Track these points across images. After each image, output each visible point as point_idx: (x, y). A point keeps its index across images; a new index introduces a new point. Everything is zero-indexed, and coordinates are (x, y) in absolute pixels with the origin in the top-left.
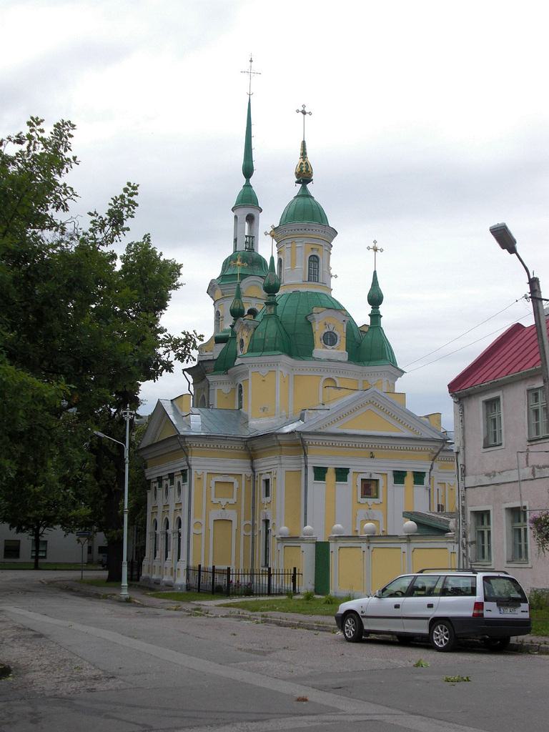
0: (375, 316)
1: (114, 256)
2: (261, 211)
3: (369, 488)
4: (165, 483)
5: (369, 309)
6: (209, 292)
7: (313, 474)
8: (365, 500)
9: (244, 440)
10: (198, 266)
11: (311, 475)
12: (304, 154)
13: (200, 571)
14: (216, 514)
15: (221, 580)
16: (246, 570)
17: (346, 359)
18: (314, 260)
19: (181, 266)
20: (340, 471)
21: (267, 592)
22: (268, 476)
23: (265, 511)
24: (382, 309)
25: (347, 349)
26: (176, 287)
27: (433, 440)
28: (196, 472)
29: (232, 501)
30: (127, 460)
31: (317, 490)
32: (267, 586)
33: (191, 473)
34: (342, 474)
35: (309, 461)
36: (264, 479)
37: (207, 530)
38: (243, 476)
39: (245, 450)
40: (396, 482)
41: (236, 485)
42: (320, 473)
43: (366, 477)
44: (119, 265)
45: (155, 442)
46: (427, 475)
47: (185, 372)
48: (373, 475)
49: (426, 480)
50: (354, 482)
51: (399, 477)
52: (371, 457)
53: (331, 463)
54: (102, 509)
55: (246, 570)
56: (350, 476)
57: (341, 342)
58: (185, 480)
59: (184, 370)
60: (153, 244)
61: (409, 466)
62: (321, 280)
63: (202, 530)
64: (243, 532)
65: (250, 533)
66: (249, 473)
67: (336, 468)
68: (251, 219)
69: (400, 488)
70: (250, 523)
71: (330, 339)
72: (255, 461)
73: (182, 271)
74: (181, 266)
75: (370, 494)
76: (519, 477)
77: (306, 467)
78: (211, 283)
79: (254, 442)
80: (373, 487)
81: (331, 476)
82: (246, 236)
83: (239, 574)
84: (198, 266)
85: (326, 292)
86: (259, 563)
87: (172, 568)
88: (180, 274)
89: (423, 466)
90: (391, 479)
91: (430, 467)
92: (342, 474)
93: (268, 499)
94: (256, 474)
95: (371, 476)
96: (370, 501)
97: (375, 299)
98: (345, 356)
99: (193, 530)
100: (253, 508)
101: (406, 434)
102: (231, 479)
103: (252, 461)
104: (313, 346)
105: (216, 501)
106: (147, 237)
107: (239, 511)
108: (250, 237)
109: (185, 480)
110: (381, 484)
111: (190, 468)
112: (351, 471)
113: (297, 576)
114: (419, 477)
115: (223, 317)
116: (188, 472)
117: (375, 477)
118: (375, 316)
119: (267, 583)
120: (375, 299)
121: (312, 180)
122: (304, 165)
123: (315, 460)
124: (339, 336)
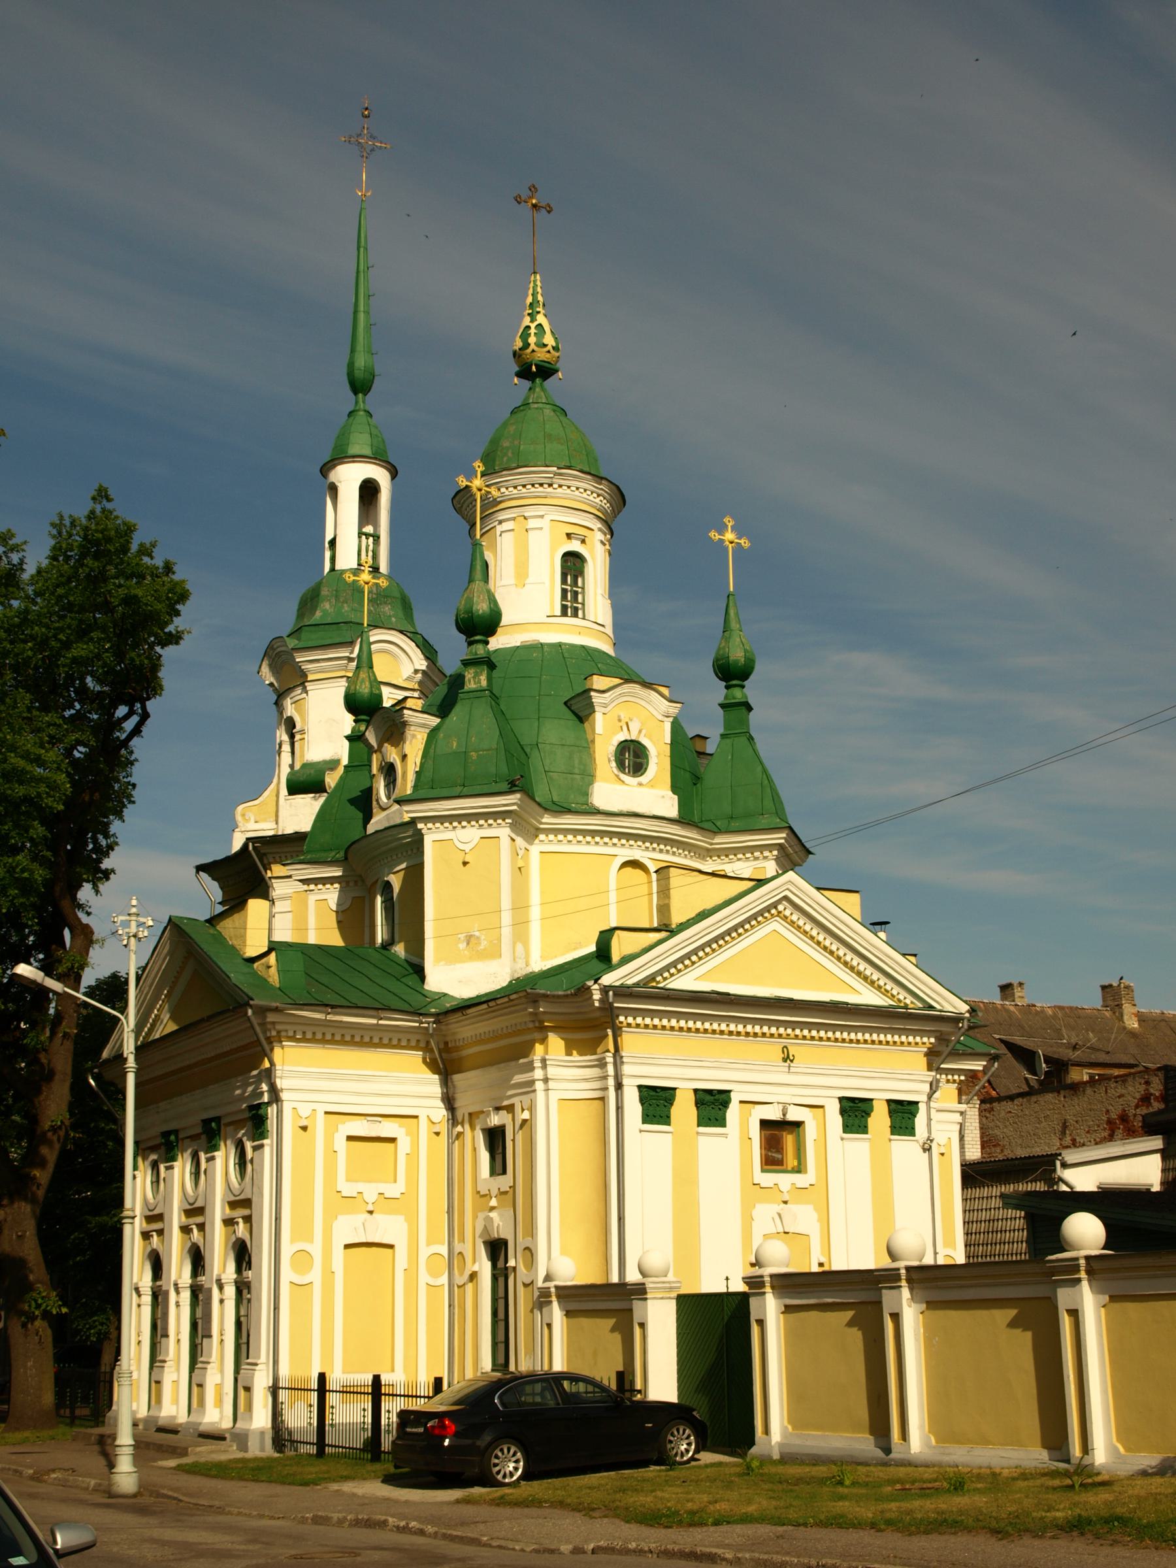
1: (721, 532)
3: (779, 1139)
7: (639, 1108)
8: (768, 1179)
14: (350, 1228)
17: (673, 813)
20: (708, 1098)
25: (675, 789)
29: (393, 1190)
30: (131, 1062)
31: (648, 1150)
35: (626, 1069)
37: (329, 1274)
38: (423, 1120)
40: (847, 1128)
41: (404, 1144)
42: (657, 1103)
43: (774, 1114)
44: (745, 543)
46: (922, 1107)
48: (791, 1109)
49: (920, 1121)
50: (742, 1127)
51: (855, 1113)
52: (785, 1060)
56: (733, 1113)
59: (200, 868)
63: (315, 1276)
65: (444, 1280)
67: (696, 1091)
69: (858, 1145)
70: (444, 1250)
75: (780, 1162)
76: (329, 1446)
77: (619, 1086)
80: (789, 1140)
81: (684, 1109)
92: (713, 1106)
96: (785, 1181)
99: (287, 1275)
100: (450, 1211)
101: (869, 997)
102: (386, 1129)
105: (348, 1189)
110: (811, 1132)
112: (735, 1098)
114: (903, 1115)
115: (302, 732)
117: (793, 1115)
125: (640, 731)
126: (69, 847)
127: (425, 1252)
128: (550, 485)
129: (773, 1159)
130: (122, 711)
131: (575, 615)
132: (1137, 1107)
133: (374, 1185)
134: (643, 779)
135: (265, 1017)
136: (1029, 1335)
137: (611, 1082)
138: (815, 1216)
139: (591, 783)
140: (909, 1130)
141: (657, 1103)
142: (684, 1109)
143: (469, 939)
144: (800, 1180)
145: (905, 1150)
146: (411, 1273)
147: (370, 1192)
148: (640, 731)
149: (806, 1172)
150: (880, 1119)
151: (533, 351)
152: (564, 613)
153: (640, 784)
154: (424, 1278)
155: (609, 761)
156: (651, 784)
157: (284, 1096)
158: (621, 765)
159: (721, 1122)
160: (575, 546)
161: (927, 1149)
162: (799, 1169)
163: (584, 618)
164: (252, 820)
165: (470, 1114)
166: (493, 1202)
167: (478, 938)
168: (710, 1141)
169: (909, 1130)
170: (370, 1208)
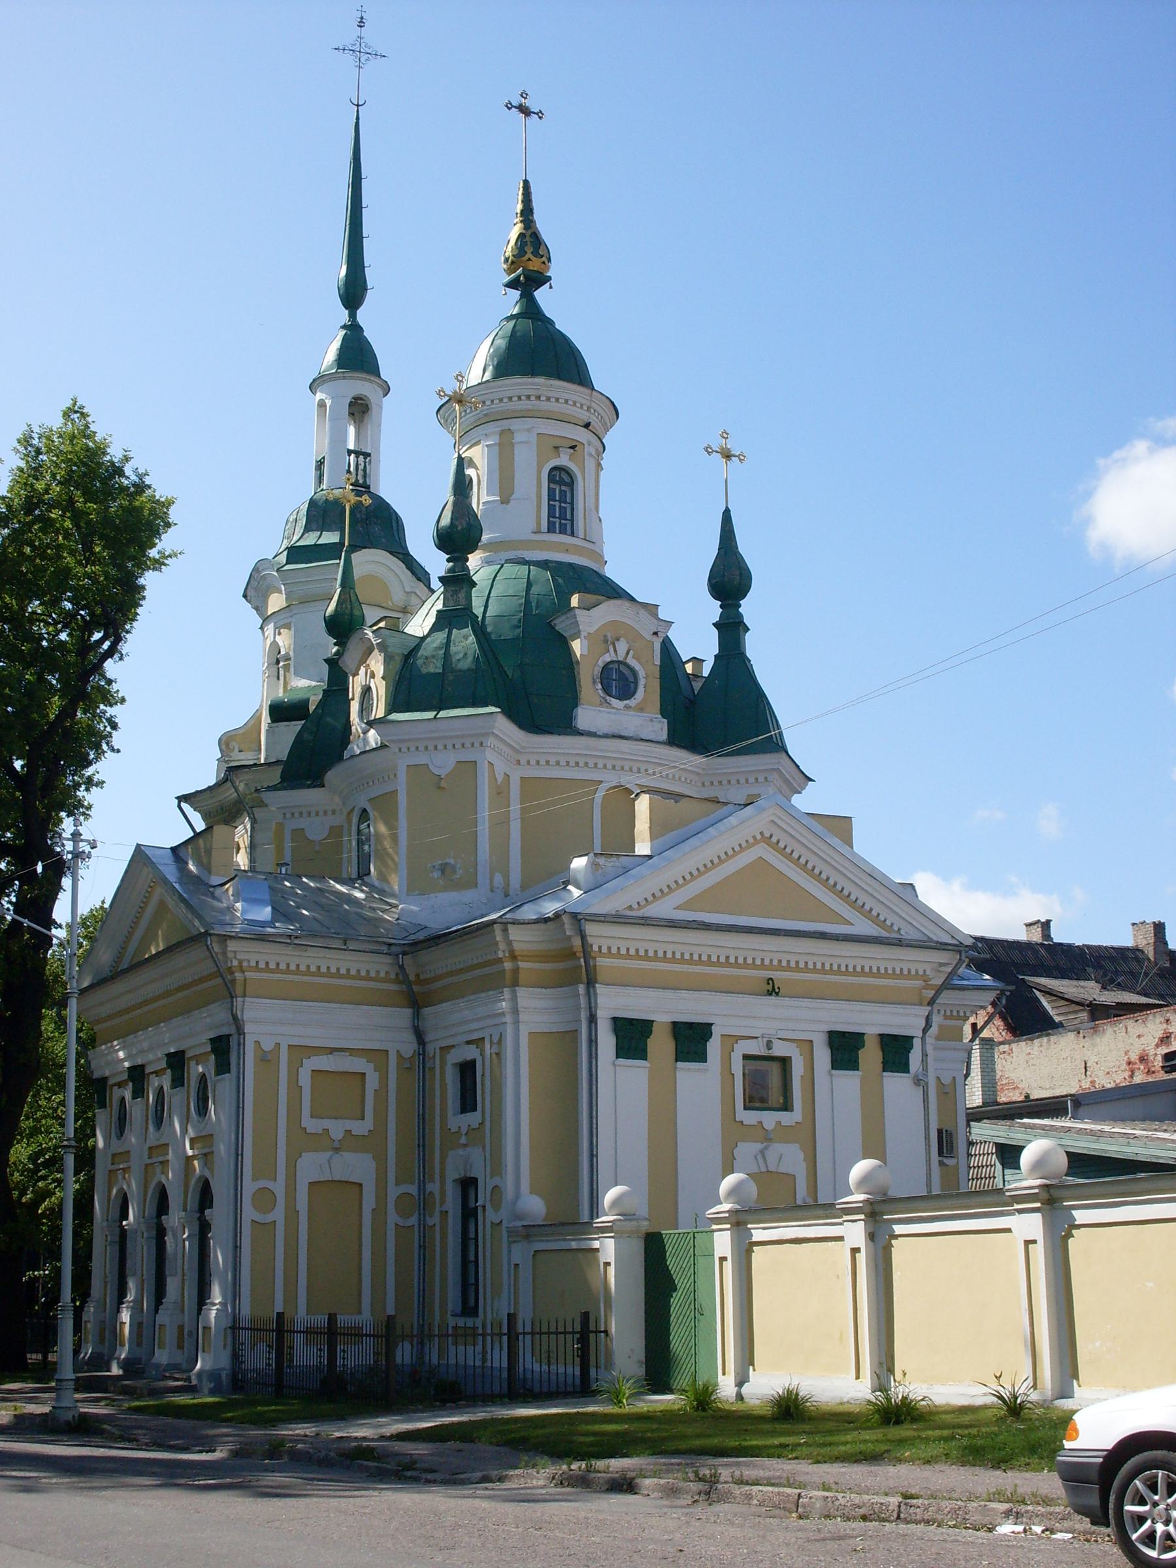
0: (731, 629)
2: (387, 390)
3: (768, 1082)
4: (154, 1082)
5: (714, 609)
6: (250, 593)
9: (393, 949)
10: (225, 513)
11: (607, 1041)
12: (527, 213)
13: (513, 1336)
15: (356, 1357)
16: (561, 1324)
17: (664, 736)
18: (562, 483)
19: (169, 503)
21: (505, 1391)
22: (471, 1053)
23: (461, 1152)
24: (748, 608)
25: (664, 713)
26: (158, 564)
27: (941, 946)
28: (257, 1043)
29: (361, 1128)
32: (505, 1375)
33: (241, 1045)
34: (691, 1040)
36: (460, 1060)
37: (292, 1214)
39: (397, 981)
42: (632, 1037)
45: (124, 965)
46: (917, 1043)
47: (183, 805)
51: (844, 1048)
53: (662, 1008)
54: (92, 756)
55: (561, 1324)
56: (714, 1047)
57: (648, 689)
58: (223, 1067)
59: (181, 799)
60: (100, 428)
61: (872, 1021)
62: (580, 531)
63: (278, 1215)
64: (393, 1218)
66: (408, 1046)
68: (359, 409)
69: (849, 1083)
70: (413, 1189)
71: (618, 682)
72: (426, 1011)
73: (173, 514)
74: (169, 503)
77: (592, 1019)
78: (256, 569)
79: (425, 956)
81: (661, 1044)
82: (350, 452)
83: (541, 1334)
84: (225, 513)
85: (594, 566)
86: (443, 1306)
87: (181, 1328)
88: (168, 525)
89: (904, 1020)
90: (823, 1056)
91: (923, 1023)
92: (691, 1040)
93: (473, 1118)
94: (430, 1049)
95: (769, 1045)
96: (770, 1119)
97: (729, 581)
98: (659, 728)
99: (249, 1213)
103: (417, 1015)
104: (575, 701)
105: (312, 1125)
106: (74, 411)
107: (381, 1160)
108: (357, 453)
109: (223, 1067)
111: (240, 1031)
113: (592, 1336)
114: (896, 1051)
116: (233, 1043)
117: (779, 1050)
118: (731, 629)
119: (505, 1364)
120: (729, 581)
121: (549, 278)
122: (528, 239)
123: (613, 1002)
124: (641, 673)
125: (628, 653)
126: (18, 764)
127: (393, 1192)
128: (538, 398)
129: (755, 1099)
130: (97, 636)
131: (563, 531)
132: (1157, 1046)
133: (340, 1122)
134: (632, 702)
135: (226, 946)
136: (1095, 535)
137: (584, 1016)
138: (801, 1155)
139: (576, 705)
140: (904, 1067)
141: (632, 1037)
142: (661, 1044)
143: (443, 869)
144: (785, 1118)
145: (896, 1085)
146: (379, 1213)
147: (337, 1129)
148: (628, 653)
149: (792, 1110)
150: (871, 1055)
151: (529, 260)
152: (551, 529)
153: (627, 707)
154: (393, 1218)
155: (594, 683)
156: (640, 708)
157: (248, 1028)
158: (607, 690)
159: (701, 1057)
160: (564, 460)
161: (917, 1081)
162: (787, 1107)
163: (572, 534)
164: (236, 750)
165: (441, 1048)
166: (463, 1140)
167: (454, 867)
168: (688, 1075)
169: (904, 1067)
170: (336, 1145)
